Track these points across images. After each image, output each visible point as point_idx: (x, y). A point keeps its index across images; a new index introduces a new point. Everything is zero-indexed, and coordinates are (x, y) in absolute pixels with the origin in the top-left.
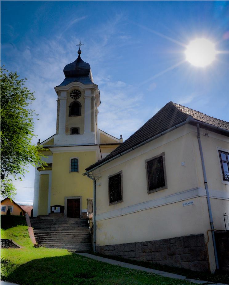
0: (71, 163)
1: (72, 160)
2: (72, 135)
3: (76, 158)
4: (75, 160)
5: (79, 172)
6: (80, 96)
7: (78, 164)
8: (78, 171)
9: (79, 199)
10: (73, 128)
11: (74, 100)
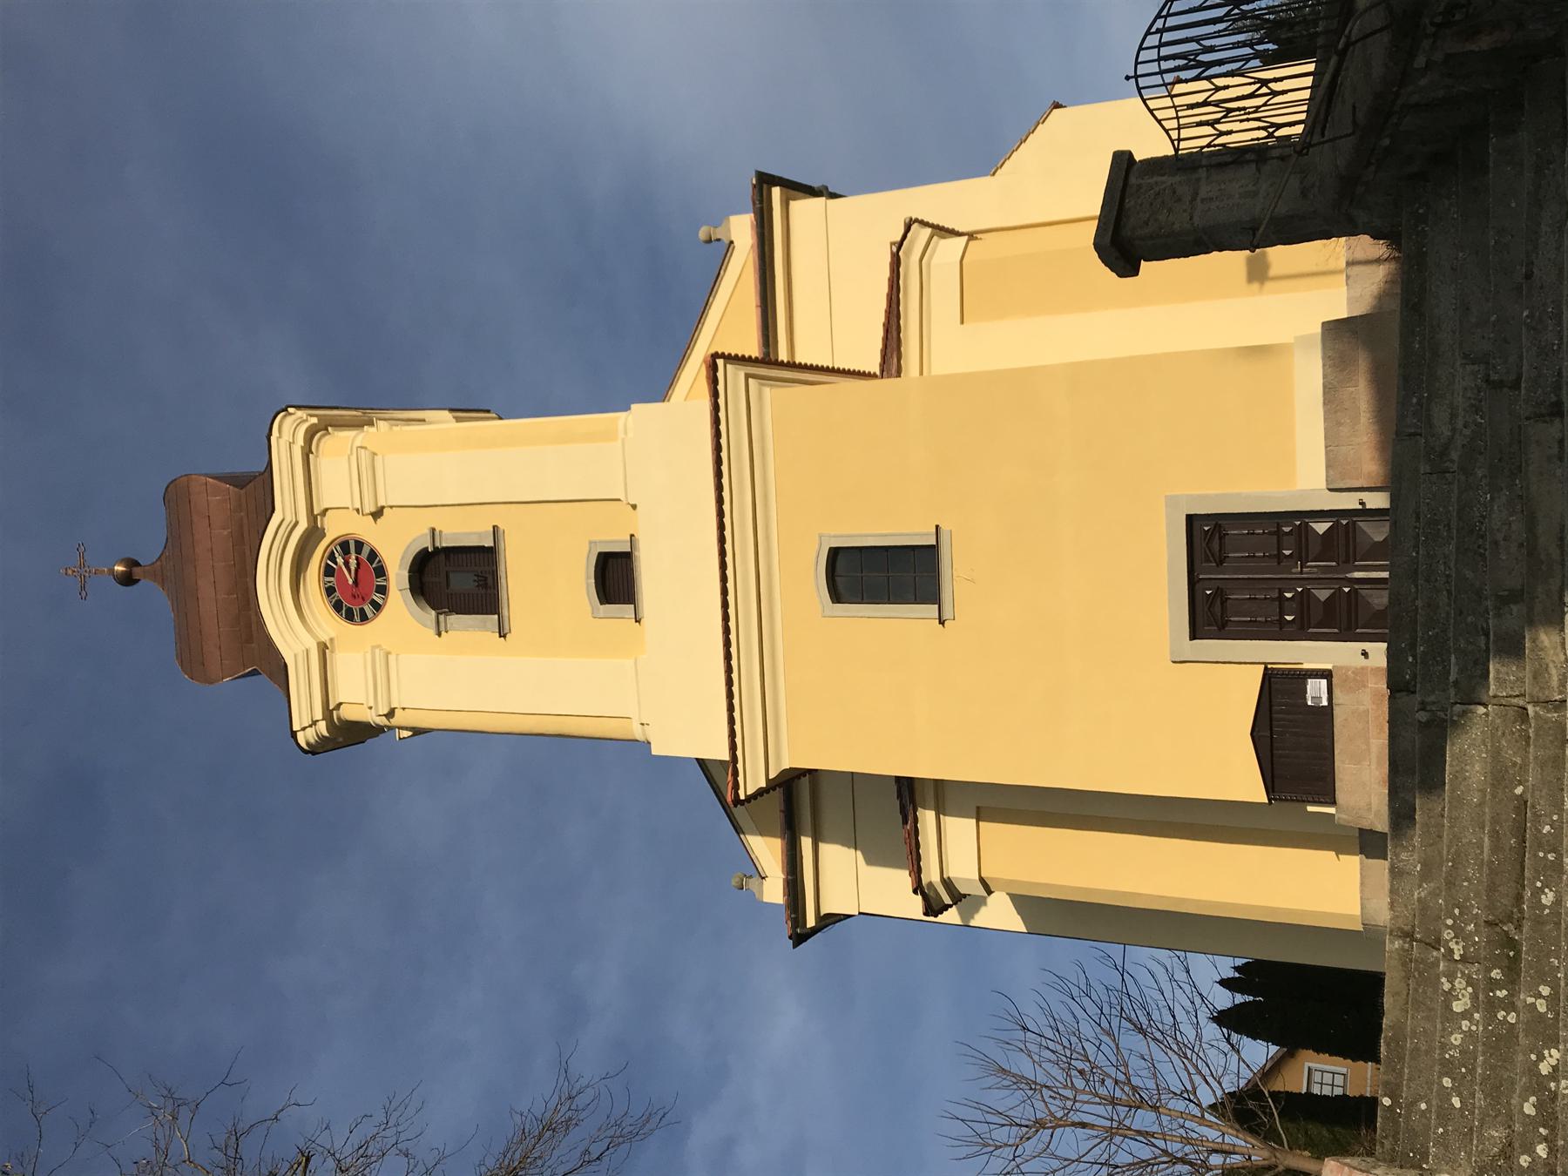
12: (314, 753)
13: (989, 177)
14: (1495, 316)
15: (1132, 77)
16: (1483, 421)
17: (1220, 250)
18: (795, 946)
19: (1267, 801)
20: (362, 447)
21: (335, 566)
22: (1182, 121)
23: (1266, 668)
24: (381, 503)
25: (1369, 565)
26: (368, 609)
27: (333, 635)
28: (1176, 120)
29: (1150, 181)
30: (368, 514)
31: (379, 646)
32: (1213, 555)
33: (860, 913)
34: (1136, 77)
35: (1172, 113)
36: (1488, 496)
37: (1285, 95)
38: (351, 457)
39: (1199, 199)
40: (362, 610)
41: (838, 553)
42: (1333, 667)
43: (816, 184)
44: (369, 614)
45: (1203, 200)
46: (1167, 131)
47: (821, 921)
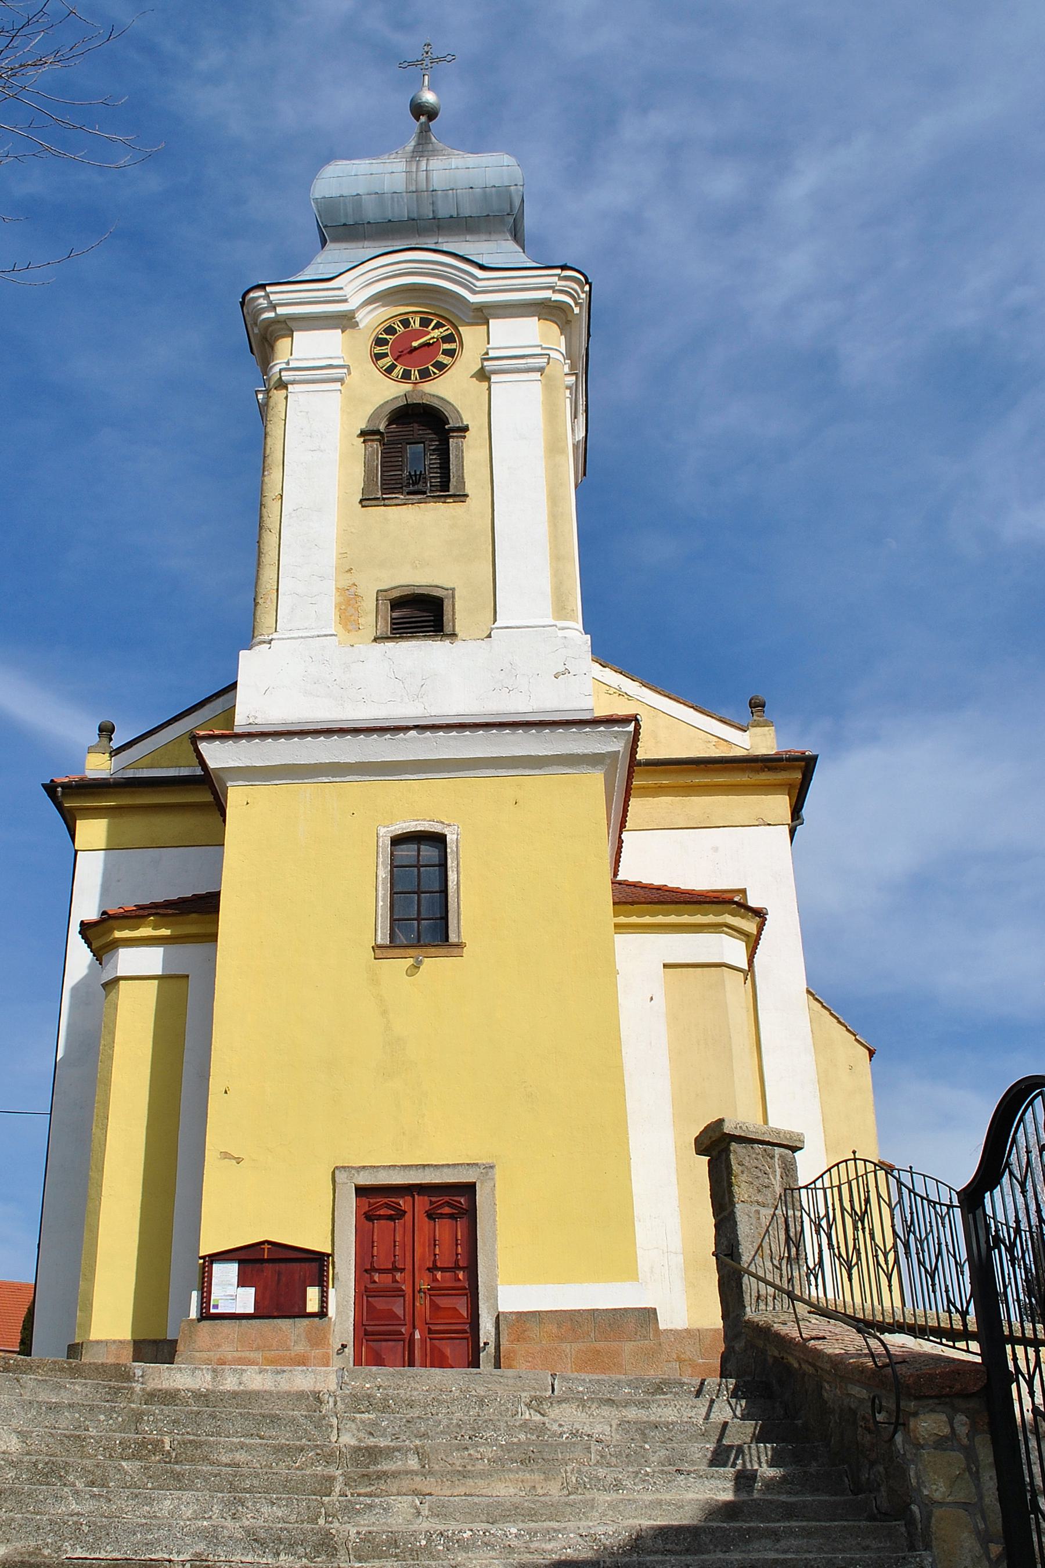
0: (384, 873)
1: (397, 841)
2: (390, 645)
3: (437, 828)
4: (429, 853)
5: (453, 635)
6: (446, 360)
7: (452, 876)
8: (453, 938)
9: (469, 1189)
10: (396, 594)
11: (407, 387)
12: (242, 304)
13: (806, 987)
14: (649, 1448)
15: (855, 1155)
16: (564, 1438)
17: (715, 1226)
18: (44, 786)
19: (201, 1255)
20: (549, 359)
21: (430, 327)
22: (829, 1191)
23: (328, 1255)
24: (494, 378)
25: (409, 1358)
26: (387, 361)
27: (361, 326)
28: (830, 1186)
29: (777, 1166)
30: (482, 364)
31: (350, 374)
32: (433, 1208)
33: (76, 852)
34: (855, 1159)
35: (836, 1183)
36: (504, 1443)
37: (847, 1279)
38: (540, 348)
39: (758, 1208)
40: (386, 355)
41: (441, 843)
42: (331, 1318)
43: (805, 812)
44: (380, 363)
45: (758, 1212)
46: (814, 1182)
47: (68, 811)
